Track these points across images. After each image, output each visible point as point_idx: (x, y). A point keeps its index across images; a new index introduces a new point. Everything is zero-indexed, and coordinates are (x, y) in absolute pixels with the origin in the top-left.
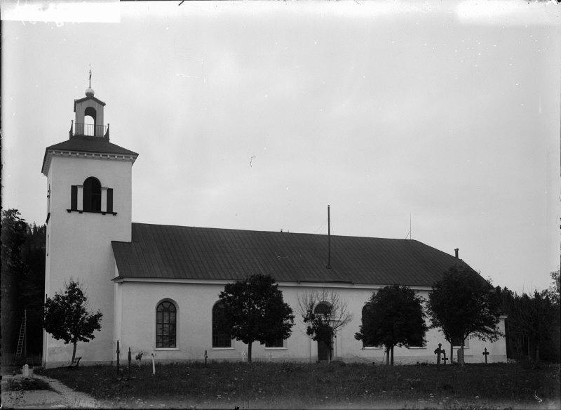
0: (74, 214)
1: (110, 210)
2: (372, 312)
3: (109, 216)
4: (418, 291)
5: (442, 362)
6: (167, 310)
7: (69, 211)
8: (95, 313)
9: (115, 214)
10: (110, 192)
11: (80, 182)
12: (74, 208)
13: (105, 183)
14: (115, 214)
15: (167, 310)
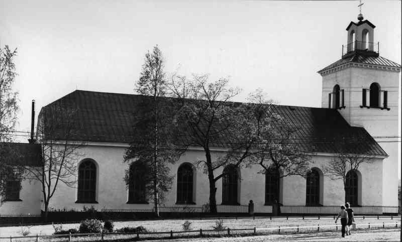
0: (365, 109)
1: (385, 107)
2: (170, 185)
3: (385, 111)
4: (22, 237)
5: (157, 95)
6: (88, 170)
7: (361, 107)
8: (4, 203)
9: (389, 109)
10: (386, 93)
11: (368, 86)
12: (364, 105)
13: (383, 86)
14: (389, 109)
15: (88, 170)
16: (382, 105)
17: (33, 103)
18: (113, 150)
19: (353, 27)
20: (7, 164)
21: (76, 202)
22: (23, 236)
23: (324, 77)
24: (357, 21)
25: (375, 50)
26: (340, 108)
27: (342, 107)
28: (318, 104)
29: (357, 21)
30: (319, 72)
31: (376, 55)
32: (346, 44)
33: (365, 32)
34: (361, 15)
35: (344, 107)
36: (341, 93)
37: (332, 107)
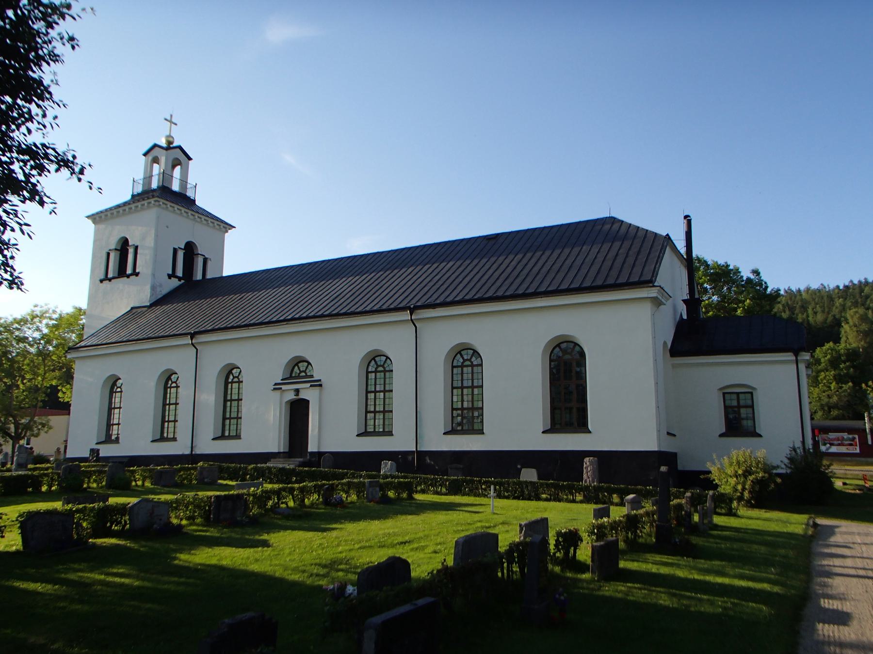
9: (101, 281)
17: (674, 435)
19: (156, 152)
22: (67, 16)
23: (102, 226)
24: (163, 143)
25: (190, 194)
27: (131, 275)
29: (163, 143)
30: (88, 217)
33: (176, 163)
36: (131, 251)
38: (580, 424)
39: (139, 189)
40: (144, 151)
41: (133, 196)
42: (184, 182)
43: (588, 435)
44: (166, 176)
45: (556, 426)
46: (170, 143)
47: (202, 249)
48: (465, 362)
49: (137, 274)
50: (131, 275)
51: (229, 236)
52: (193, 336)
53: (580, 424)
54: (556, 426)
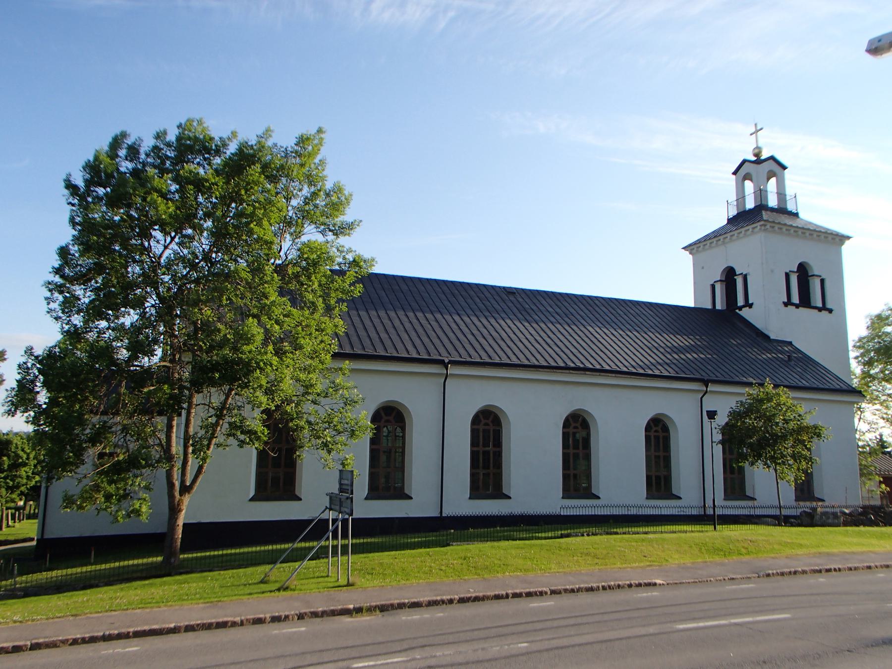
9: (830, 311)
16: (820, 305)
18: (558, 388)
20: (282, 293)
21: (252, 500)
25: (790, 207)
26: (740, 308)
27: (744, 306)
28: (688, 301)
31: (796, 215)
32: (733, 197)
33: (771, 175)
34: (757, 147)
35: (750, 306)
37: (719, 306)
38: (499, 493)
39: (733, 212)
40: (733, 170)
41: (728, 220)
42: (781, 195)
43: (409, 501)
44: (761, 193)
45: (263, 492)
46: (757, 155)
47: (816, 268)
48: (488, 429)
49: (751, 306)
50: (744, 306)
51: (846, 248)
52: (706, 383)
53: (499, 493)
54: (263, 492)
